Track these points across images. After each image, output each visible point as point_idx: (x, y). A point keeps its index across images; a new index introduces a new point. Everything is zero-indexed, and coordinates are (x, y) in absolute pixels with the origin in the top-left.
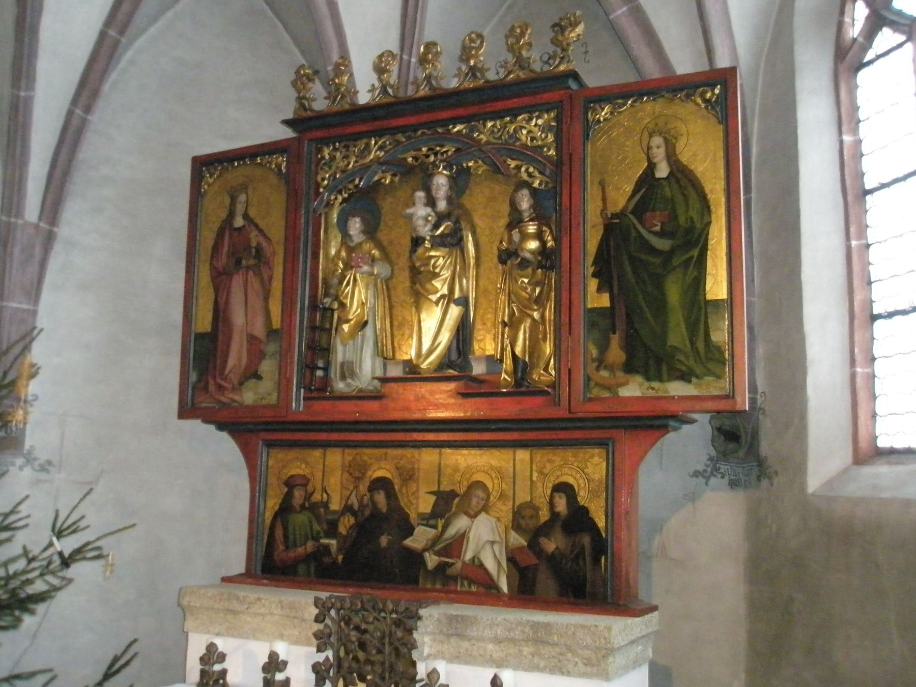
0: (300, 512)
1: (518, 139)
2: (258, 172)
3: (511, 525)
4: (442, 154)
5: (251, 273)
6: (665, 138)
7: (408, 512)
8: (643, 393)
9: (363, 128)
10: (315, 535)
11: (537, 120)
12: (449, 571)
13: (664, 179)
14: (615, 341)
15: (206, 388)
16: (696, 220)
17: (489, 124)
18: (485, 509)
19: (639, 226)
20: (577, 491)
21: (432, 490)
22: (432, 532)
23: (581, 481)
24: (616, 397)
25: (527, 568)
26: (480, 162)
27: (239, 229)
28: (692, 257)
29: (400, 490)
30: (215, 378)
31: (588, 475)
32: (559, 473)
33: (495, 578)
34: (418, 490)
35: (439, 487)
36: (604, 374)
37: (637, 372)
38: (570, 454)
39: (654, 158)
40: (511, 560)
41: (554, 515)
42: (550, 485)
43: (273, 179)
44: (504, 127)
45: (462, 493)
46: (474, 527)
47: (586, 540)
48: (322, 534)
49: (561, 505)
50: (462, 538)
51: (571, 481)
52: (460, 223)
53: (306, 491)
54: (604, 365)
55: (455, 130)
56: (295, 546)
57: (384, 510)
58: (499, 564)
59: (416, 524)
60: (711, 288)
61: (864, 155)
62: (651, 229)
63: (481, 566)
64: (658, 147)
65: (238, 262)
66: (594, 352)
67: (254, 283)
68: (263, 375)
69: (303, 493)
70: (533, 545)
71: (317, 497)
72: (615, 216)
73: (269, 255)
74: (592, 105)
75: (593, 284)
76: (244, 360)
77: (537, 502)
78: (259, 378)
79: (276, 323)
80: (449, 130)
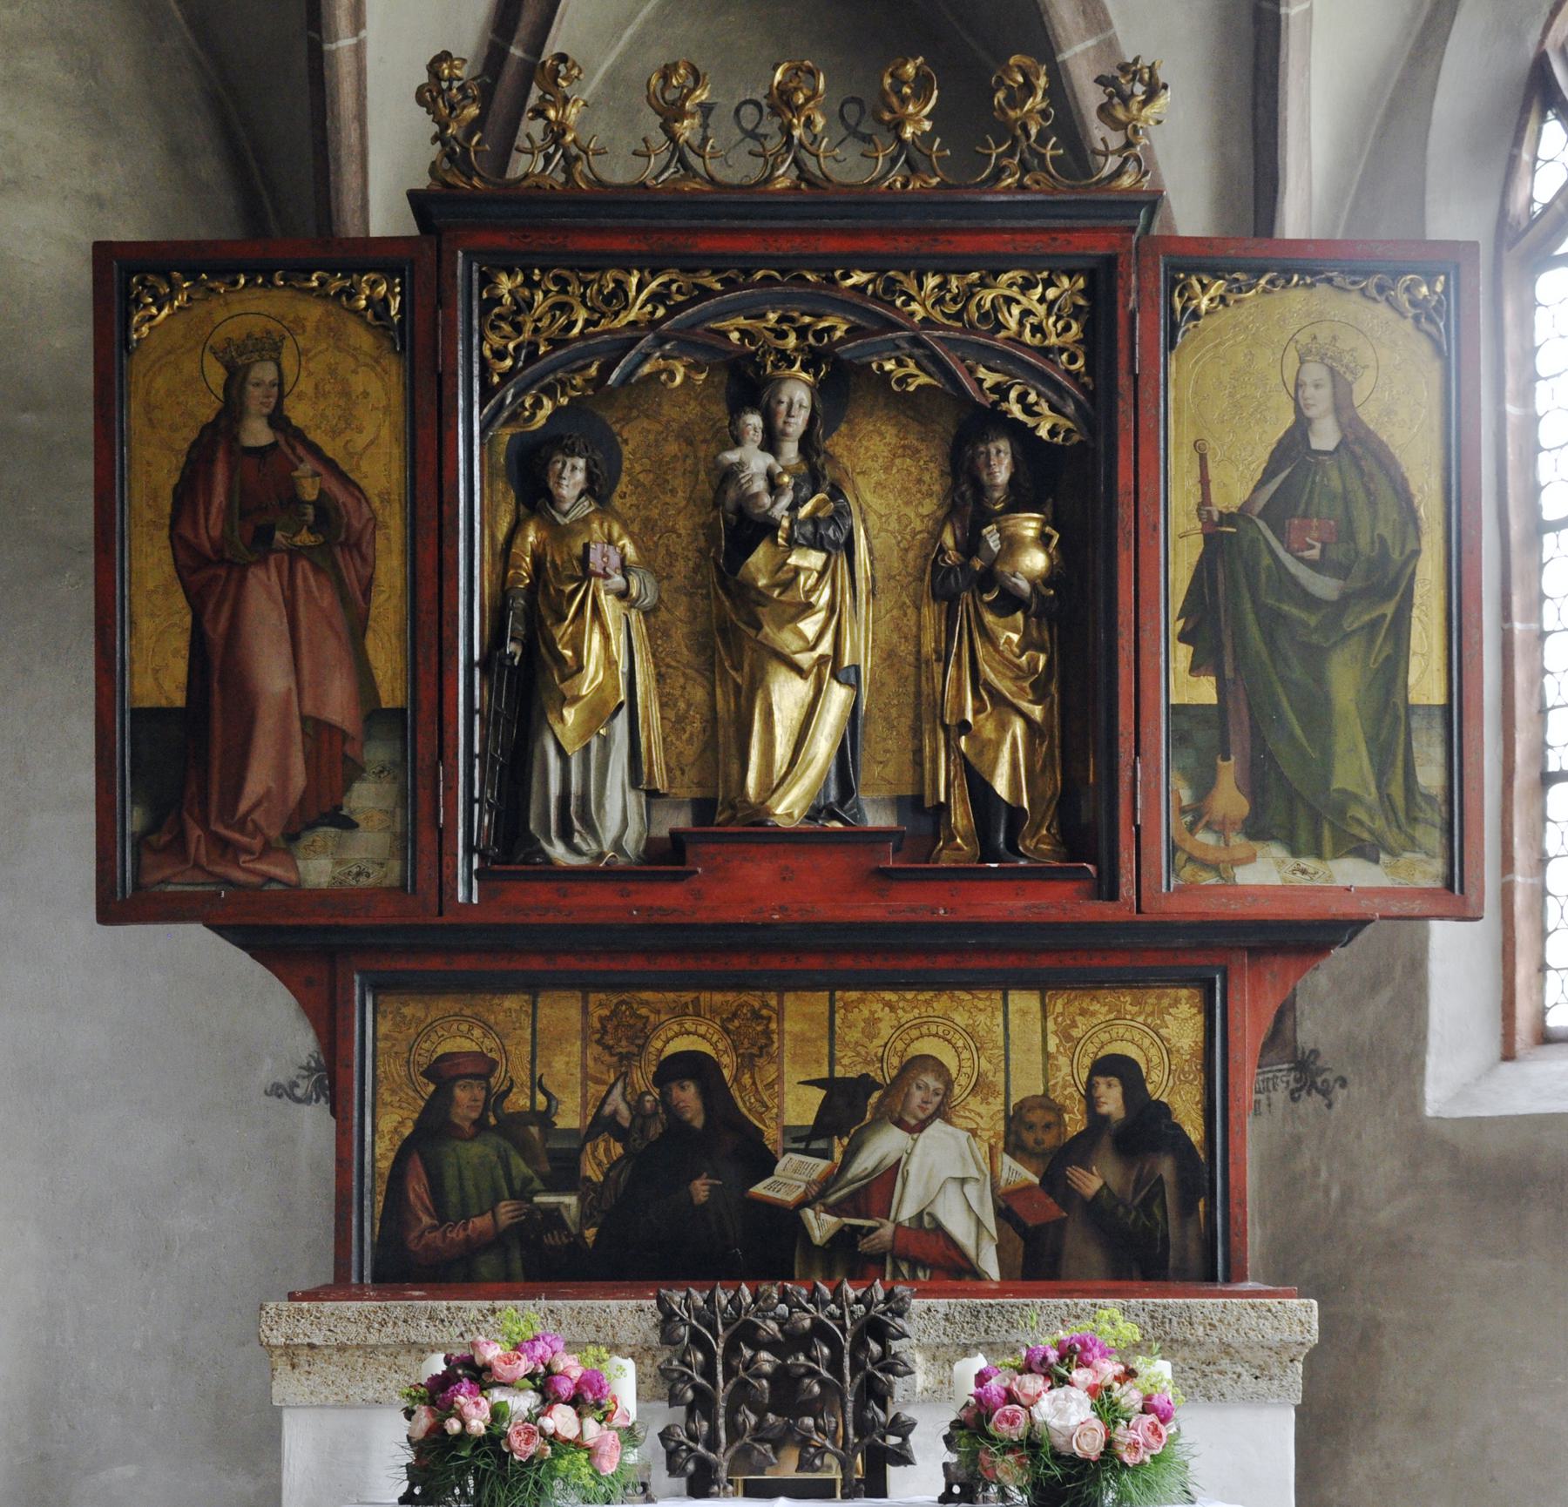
0: (472, 1139)
1: (1001, 326)
2: (313, 312)
3: (1001, 1145)
4: (819, 335)
5: (303, 566)
6: (1331, 369)
7: (761, 1126)
8: (1284, 879)
9: (620, 245)
10: (517, 1185)
11: (1045, 289)
12: (864, 1245)
13: (1325, 453)
14: (1228, 774)
15: (178, 847)
16: (1390, 543)
17: (931, 282)
18: (943, 1112)
19: (1275, 543)
20: (1144, 1071)
21: (815, 1076)
22: (823, 1164)
23: (1153, 1052)
24: (1230, 883)
25: (1039, 1229)
26: (911, 363)
27: (260, 452)
28: (1384, 616)
29: (736, 1079)
30: (204, 822)
31: (1168, 1040)
32: (1105, 1037)
33: (972, 1252)
34: (780, 1078)
35: (831, 1070)
36: (1205, 837)
37: (1272, 838)
38: (1128, 999)
39: (1308, 406)
40: (1004, 1213)
41: (1097, 1122)
42: (1087, 1061)
43: (363, 339)
44: (969, 293)
45: (888, 1081)
46: (918, 1151)
47: (1166, 1168)
48: (537, 1184)
49: (1112, 1100)
50: (889, 1176)
51: (1133, 1052)
52: (842, 495)
53: (488, 1089)
54: (1204, 821)
55: (849, 282)
56: (466, 1216)
57: (698, 1122)
58: (979, 1223)
59: (780, 1151)
60: (1418, 681)
61: (1543, 450)
62: (1300, 554)
63: (939, 1229)
64: (1317, 386)
65: (262, 539)
66: (1186, 796)
67: (316, 592)
68: (357, 818)
69: (482, 1095)
70: (1054, 1181)
71: (519, 1101)
72: (1227, 518)
73: (357, 525)
74: (1182, 276)
75: (1182, 654)
76: (299, 780)
77: (1057, 1096)
78: (349, 824)
79: (391, 692)
80: (832, 281)
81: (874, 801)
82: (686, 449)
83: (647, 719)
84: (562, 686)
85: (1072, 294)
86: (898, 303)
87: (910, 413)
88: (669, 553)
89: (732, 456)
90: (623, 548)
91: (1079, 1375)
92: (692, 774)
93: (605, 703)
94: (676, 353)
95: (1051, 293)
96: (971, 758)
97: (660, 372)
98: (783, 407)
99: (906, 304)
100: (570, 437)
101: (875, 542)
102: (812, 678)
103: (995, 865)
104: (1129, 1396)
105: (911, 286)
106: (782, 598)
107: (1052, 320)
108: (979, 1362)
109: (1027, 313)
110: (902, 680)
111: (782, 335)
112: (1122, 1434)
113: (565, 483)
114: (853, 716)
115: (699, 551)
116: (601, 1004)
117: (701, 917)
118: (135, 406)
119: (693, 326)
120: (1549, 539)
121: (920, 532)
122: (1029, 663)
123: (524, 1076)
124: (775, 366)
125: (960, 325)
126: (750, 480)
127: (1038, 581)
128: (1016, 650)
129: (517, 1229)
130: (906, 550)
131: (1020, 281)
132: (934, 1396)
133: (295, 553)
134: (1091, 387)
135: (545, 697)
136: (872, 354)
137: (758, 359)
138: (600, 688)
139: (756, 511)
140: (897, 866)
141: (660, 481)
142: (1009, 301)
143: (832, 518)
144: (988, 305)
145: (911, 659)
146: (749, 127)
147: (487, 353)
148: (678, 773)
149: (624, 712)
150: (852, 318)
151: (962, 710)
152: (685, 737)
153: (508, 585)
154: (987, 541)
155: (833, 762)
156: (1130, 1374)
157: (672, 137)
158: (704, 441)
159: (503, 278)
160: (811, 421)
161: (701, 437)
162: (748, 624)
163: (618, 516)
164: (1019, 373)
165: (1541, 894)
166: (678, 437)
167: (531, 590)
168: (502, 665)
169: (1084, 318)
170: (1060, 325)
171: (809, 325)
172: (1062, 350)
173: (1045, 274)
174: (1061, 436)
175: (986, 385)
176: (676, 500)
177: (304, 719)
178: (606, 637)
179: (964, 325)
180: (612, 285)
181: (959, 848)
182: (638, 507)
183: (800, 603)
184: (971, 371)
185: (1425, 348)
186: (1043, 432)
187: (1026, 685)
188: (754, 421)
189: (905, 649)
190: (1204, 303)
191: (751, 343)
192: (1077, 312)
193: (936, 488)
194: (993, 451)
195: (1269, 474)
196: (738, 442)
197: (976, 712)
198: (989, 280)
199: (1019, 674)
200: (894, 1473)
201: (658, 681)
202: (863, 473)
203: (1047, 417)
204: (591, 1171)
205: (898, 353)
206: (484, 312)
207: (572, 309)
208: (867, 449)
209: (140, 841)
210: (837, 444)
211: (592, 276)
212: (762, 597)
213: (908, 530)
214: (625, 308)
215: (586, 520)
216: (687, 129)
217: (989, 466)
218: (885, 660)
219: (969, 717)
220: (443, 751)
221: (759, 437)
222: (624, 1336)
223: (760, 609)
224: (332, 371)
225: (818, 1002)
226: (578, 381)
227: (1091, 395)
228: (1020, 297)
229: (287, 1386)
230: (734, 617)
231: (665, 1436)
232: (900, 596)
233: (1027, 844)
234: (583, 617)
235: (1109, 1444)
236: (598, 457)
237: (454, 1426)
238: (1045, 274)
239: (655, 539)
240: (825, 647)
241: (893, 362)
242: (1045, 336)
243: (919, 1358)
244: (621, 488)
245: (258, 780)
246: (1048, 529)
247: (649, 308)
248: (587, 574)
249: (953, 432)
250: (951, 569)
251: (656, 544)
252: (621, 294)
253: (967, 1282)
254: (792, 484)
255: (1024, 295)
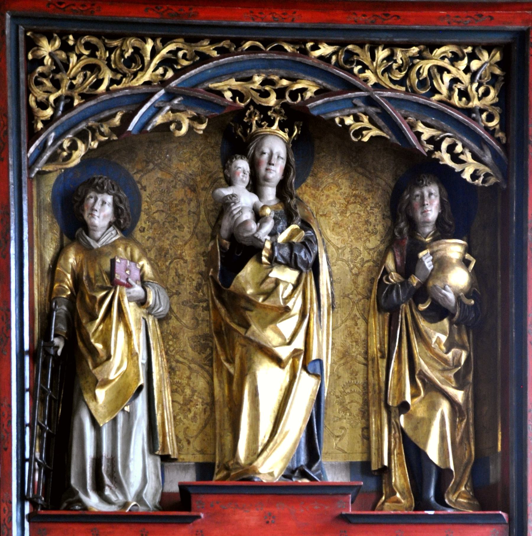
1: (434, 91)
4: (294, 95)
17: (382, 54)
26: (365, 119)
55: (317, 53)
80: (304, 52)
81: (332, 465)
82: (191, 195)
83: (161, 402)
84: (94, 371)
85: (491, 65)
86: (356, 69)
87: (360, 170)
88: (178, 275)
89: (226, 192)
90: (142, 267)
92: (196, 444)
93: (129, 386)
94: (182, 108)
95: (475, 65)
96: (409, 433)
97: (171, 123)
98: (265, 157)
99: (362, 71)
100: (100, 178)
101: (334, 268)
102: (288, 367)
103: (432, 513)
105: (365, 57)
106: (266, 303)
107: (475, 85)
109: (455, 80)
110: (354, 374)
111: (266, 94)
113: (96, 214)
115: (201, 273)
119: (196, 86)
121: (368, 261)
122: (453, 358)
124: (259, 125)
125: (403, 89)
126: (241, 211)
127: (462, 294)
128: (444, 348)
130: (357, 275)
131: (450, 55)
134: (504, 141)
135: (82, 382)
136: (335, 111)
137: (245, 120)
138: (125, 375)
139: (246, 235)
140: (353, 513)
141: (170, 219)
142: (441, 70)
143: (303, 243)
144: (425, 74)
145: (361, 358)
147: (33, 104)
148: (185, 443)
149: (143, 395)
150: (320, 82)
151: (402, 394)
152: (190, 415)
153: (54, 296)
154: (422, 262)
155: (303, 435)
158: (204, 189)
159: (44, 42)
160: (286, 171)
161: (202, 186)
162: (239, 325)
163: (137, 243)
164: (449, 127)
166: (185, 185)
167: (72, 299)
168: (47, 354)
169: (499, 85)
170: (481, 90)
171: (285, 88)
172: (482, 111)
173: (469, 49)
174: (481, 179)
175: (424, 137)
176: (183, 234)
178: (129, 334)
179: (407, 90)
180: (131, 51)
181: (398, 501)
182: (154, 239)
183: (279, 308)
184: (412, 126)
186: (467, 176)
187: (451, 375)
189: (357, 351)
191: (241, 101)
193: (379, 228)
194: (426, 194)
196: (230, 183)
197: (413, 396)
198: (426, 54)
201: (169, 373)
202: (325, 215)
203: (470, 164)
205: (355, 111)
207: (99, 70)
208: (328, 196)
211: (115, 43)
212: (251, 303)
213: (358, 260)
214: (142, 70)
215: (114, 245)
217: (423, 205)
218: (341, 359)
219: (408, 398)
221: (247, 179)
223: (248, 313)
226: (105, 129)
228: (450, 68)
230: (228, 320)
232: (352, 309)
233: (450, 498)
234: (111, 317)
236: (123, 195)
238: (469, 49)
239: (167, 264)
240: (299, 343)
241: (351, 117)
242: (469, 99)
244: (141, 224)
246: (467, 256)
247: (161, 70)
248: (114, 283)
249: (393, 185)
250: (393, 286)
251: (168, 268)
252: (138, 59)
254: (273, 215)
255: (453, 66)
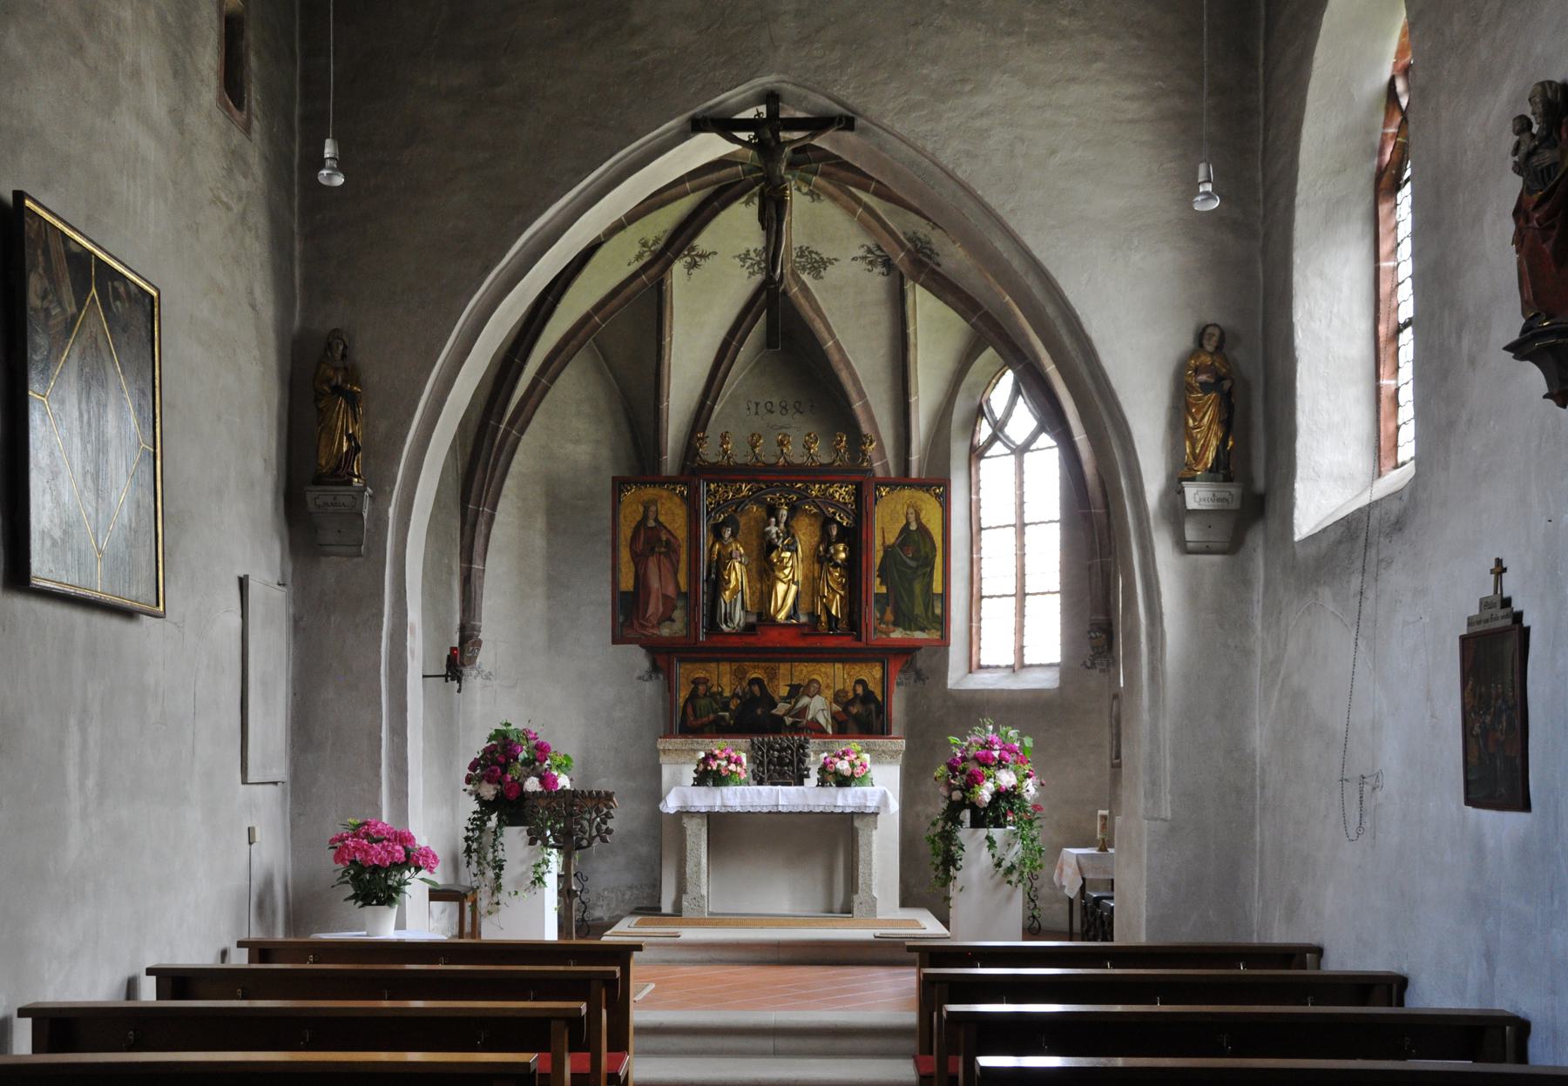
1: (835, 497)
2: (665, 493)
5: (662, 557)
6: (915, 511)
12: (799, 725)
14: (889, 610)
17: (817, 486)
18: (819, 693)
22: (789, 705)
27: (652, 528)
29: (768, 684)
30: (637, 619)
40: (833, 717)
41: (856, 695)
43: (677, 500)
44: (827, 489)
47: (873, 707)
49: (860, 690)
50: (805, 708)
63: (818, 722)
65: (653, 549)
66: (878, 615)
70: (845, 710)
71: (715, 689)
72: (889, 547)
75: (878, 581)
76: (661, 609)
77: (847, 689)
78: (673, 621)
91: (846, 758)
104: (858, 763)
108: (825, 754)
110: (809, 583)
111: (780, 499)
112: (856, 770)
114: (797, 594)
116: (735, 666)
117: (760, 645)
118: (622, 516)
120: (983, 532)
123: (716, 683)
129: (714, 721)
132: (815, 763)
133: (660, 553)
146: (769, 408)
156: (858, 758)
157: (754, 452)
160: (787, 518)
165: (980, 628)
177: (662, 594)
185: (938, 505)
186: (845, 524)
188: (773, 520)
189: (810, 575)
190: (884, 494)
192: (853, 494)
195: (900, 535)
196: (769, 525)
199: (838, 584)
200: (805, 780)
204: (732, 707)
206: (707, 493)
209: (622, 625)
210: (793, 523)
212: (775, 564)
216: (757, 450)
220: (696, 604)
222: (743, 748)
224: (670, 508)
225: (788, 666)
227: (857, 516)
229: (663, 759)
231: (752, 771)
235: (852, 773)
237: (709, 768)
240: (790, 577)
243: (812, 754)
245: (651, 610)
253: (824, 735)
